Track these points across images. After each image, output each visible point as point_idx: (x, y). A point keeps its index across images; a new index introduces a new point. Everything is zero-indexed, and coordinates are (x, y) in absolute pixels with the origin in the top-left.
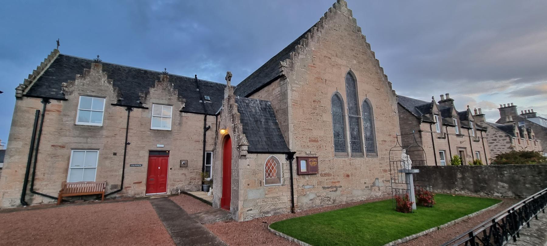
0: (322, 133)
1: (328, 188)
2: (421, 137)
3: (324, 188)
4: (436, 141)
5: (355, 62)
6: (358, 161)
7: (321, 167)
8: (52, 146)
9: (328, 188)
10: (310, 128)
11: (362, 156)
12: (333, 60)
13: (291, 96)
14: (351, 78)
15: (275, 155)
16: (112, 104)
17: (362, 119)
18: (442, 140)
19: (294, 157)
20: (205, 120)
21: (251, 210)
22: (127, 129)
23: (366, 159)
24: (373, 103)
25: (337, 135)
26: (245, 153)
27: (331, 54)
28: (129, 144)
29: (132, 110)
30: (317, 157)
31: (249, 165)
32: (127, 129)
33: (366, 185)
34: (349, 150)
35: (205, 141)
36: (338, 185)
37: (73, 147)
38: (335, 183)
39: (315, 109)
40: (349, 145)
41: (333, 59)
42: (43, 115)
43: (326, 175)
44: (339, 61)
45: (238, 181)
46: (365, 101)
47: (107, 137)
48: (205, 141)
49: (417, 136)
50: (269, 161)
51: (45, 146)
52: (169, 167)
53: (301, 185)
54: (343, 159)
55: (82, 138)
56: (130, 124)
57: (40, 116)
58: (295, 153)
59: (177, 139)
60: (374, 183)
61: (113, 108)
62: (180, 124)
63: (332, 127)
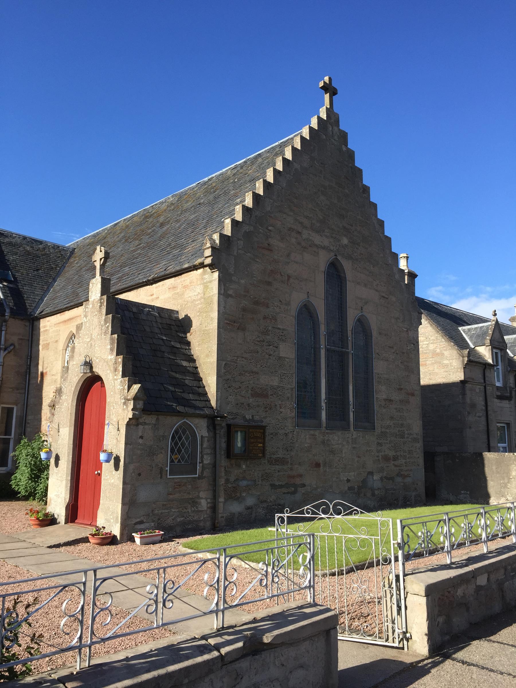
0: (275, 382)
1: (281, 486)
4: (495, 404)
6: (336, 438)
9: (281, 486)
10: (255, 369)
11: (346, 428)
12: (304, 236)
14: (335, 275)
17: (350, 356)
18: (505, 404)
23: (353, 433)
24: (374, 323)
25: (302, 385)
27: (301, 223)
31: (141, 437)
33: (349, 485)
36: (298, 481)
38: (293, 477)
41: (305, 234)
44: (317, 239)
46: (359, 320)
53: (232, 478)
54: (312, 432)
60: (364, 481)
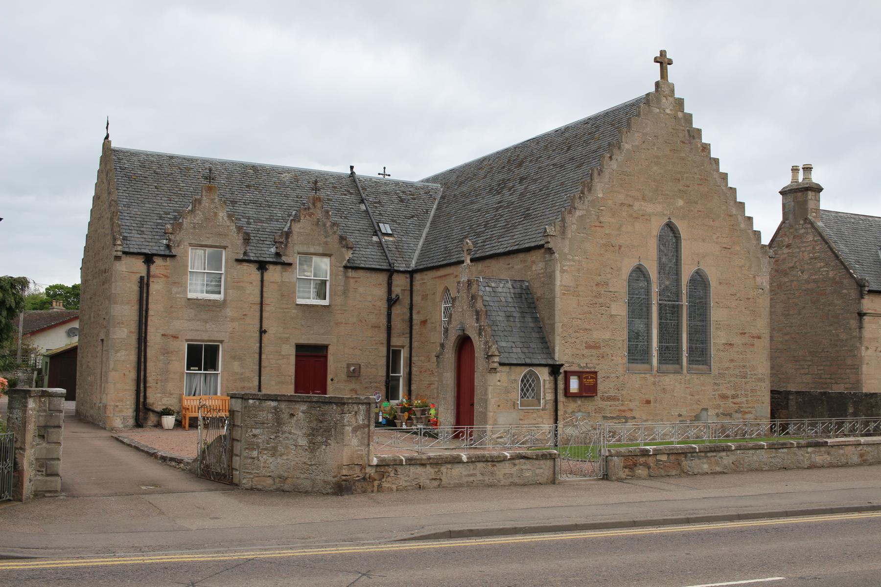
0: (607, 335)
1: (612, 418)
2: (861, 328)
3: (605, 418)
5: (681, 203)
6: (668, 380)
7: (601, 387)
8: (163, 335)
9: (612, 418)
10: (588, 327)
11: (679, 372)
12: (635, 208)
13: (561, 280)
15: (533, 369)
16: (237, 260)
19: (562, 371)
20: (390, 285)
21: (501, 437)
22: (261, 304)
26: (496, 365)
27: (632, 197)
28: (265, 332)
29: (267, 269)
30: (596, 373)
32: (261, 304)
34: (655, 361)
35: (389, 329)
36: (628, 414)
37: (188, 338)
38: (624, 411)
39: (599, 295)
40: (655, 353)
41: (637, 206)
42: (148, 285)
43: (609, 398)
44: (649, 208)
45: (486, 401)
47: (233, 320)
48: (389, 329)
49: (854, 323)
50: (525, 376)
51: (154, 337)
52: (329, 378)
53: (569, 411)
55: (199, 323)
56: (265, 295)
57: (144, 285)
58: (562, 365)
59: (342, 323)
61: (239, 267)
62: (345, 293)
63: (625, 325)
